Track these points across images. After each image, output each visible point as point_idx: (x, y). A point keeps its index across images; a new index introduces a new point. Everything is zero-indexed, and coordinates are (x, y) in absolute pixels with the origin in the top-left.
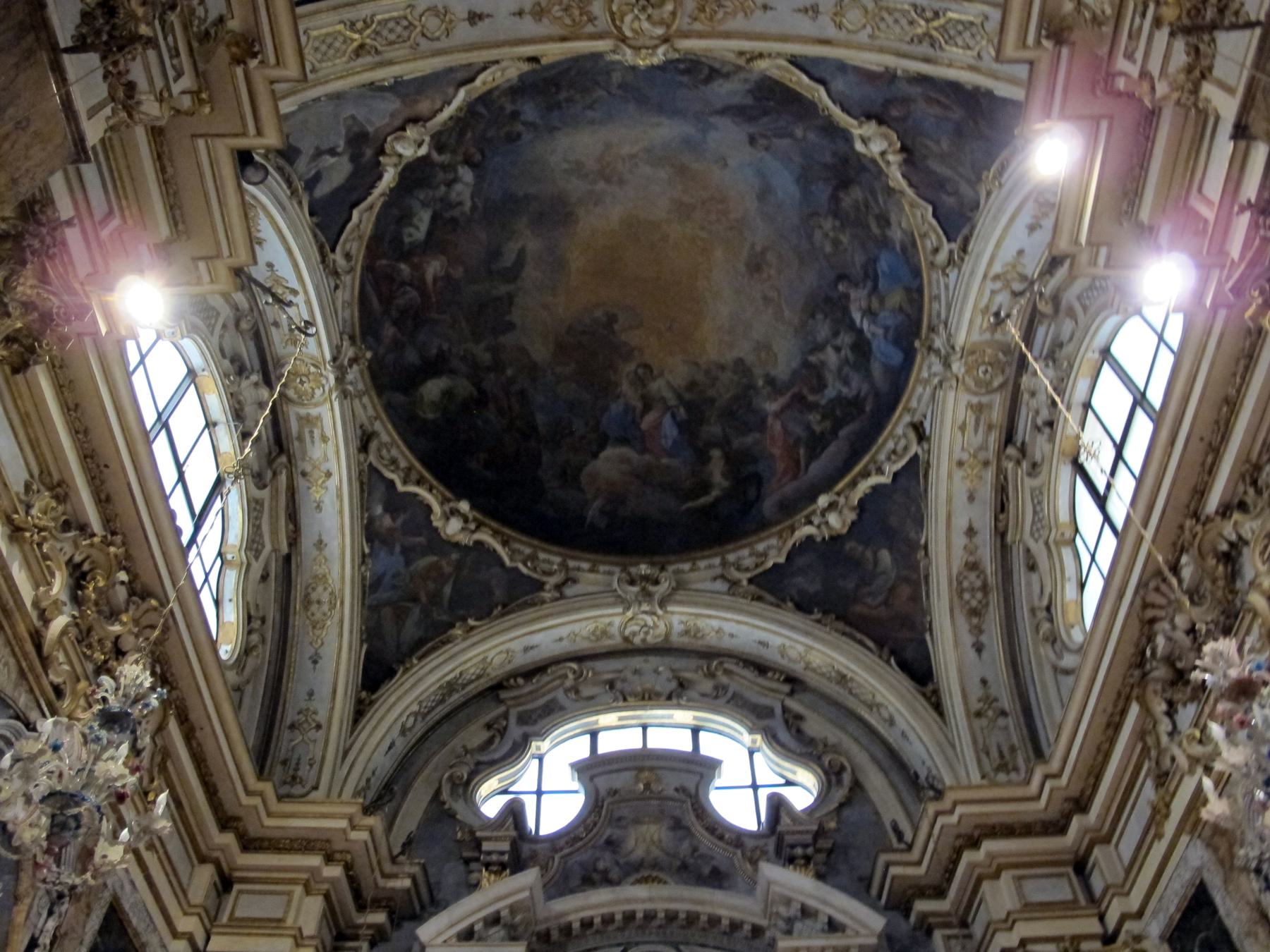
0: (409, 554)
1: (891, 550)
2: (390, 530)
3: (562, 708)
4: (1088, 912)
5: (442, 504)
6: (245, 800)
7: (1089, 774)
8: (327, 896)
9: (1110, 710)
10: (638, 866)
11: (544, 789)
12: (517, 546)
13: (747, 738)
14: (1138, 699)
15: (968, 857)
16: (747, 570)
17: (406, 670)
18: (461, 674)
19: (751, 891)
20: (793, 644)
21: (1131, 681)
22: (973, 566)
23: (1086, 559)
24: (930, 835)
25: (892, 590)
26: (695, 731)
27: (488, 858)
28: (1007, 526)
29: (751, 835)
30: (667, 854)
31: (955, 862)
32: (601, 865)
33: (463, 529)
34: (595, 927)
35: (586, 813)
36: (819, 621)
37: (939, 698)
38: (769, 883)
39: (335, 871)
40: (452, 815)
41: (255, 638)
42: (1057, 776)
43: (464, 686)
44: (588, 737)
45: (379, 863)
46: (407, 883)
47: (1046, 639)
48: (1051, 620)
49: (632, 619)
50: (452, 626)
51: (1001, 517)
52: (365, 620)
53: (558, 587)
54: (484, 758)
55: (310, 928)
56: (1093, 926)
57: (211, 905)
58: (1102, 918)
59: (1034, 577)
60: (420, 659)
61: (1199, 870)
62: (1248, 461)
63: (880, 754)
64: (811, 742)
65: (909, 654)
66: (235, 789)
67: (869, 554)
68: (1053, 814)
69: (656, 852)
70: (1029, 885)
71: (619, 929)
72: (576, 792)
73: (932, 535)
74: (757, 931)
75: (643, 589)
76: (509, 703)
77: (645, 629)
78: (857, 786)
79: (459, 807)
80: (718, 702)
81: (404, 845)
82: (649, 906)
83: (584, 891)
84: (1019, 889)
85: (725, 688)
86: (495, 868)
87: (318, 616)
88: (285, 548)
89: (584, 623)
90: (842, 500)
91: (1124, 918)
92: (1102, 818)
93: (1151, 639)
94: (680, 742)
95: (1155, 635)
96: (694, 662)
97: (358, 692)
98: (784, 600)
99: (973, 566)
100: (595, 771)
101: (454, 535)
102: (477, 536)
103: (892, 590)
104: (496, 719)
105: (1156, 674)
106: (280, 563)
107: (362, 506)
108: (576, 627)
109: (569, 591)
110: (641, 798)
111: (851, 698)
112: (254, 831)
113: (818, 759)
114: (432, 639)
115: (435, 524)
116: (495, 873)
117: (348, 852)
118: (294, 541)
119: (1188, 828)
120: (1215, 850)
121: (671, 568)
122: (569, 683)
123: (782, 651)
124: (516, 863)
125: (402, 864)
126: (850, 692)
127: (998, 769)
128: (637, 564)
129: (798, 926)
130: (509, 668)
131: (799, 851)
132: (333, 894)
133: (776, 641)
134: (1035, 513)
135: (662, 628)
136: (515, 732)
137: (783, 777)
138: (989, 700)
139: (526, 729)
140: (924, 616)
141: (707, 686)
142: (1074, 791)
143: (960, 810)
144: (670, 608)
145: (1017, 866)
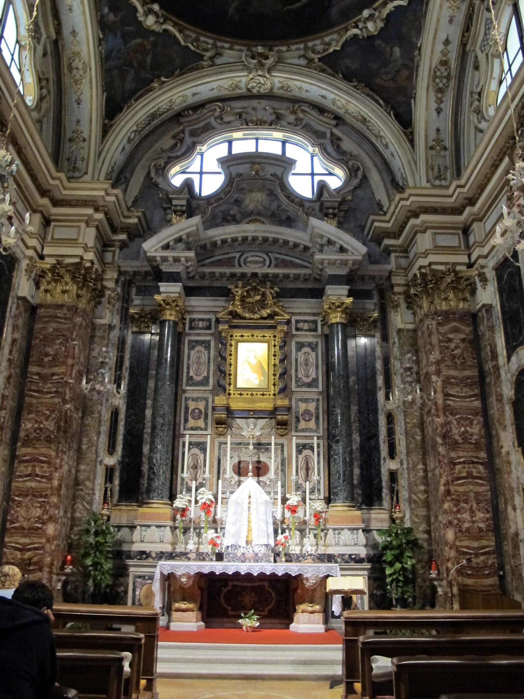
0: (126, 37)
1: (400, 47)
2: (114, 22)
3: (213, 128)
5: (143, 6)
6: (52, 182)
8: (97, 228)
9: (495, 157)
10: (251, 213)
11: (204, 171)
12: (188, 32)
13: (311, 149)
14: (509, 155)
15: (413, 221)
16: (318, 53)
17: (129, 107)
18: (159, 109)
19: (305, 229)
20: (340, 99)
21: (508, 145)
24: (394, 212)
25: (398, 71)
26: (284, 143)
27: (176, 208)
28: (468, 40)
30: (265, 208)
31: (406, 223)
32: (232, 213)
33: (156, 22)
34: (228, 243)
35: (224, 186)
36: (355, 87)
37: (413, 136)
38: (313, 227)
39: (100, 216)
40: (156, 185)
41: (44, 91)
42: (463, 186)
43: (160, 115)
44: (227, 144)
45: (122, 212)
46: (136, 220)
47: (475, 111)
48: (479, 101)
49: (252, 79)
50: (152, 81)
51: (466, 34)
52: (104, 79)
53: (211, 58)
54: (171, 155)
55: (91, 244)
56: (464, 259)
57: (42, 232)
58: (469, 256)
59: (477, 73)
60: (136, 100)
63: (379, 161)
64: (343, 153)
66: (46, 177)
67: (388, 49)
68: (458, 204)
69: (260, 208)
70: (439, 237)
71: (240, 244)
72: (220, 173)
73: (424, 42)
74: (306, 249)
75: (260, 62)
76: (185, 124)
77: (259, 85)
78: (365, 178)
79: (159, 180)
80: (296, 128)
81: (133, 202)
82: (254, 234)
83: (223, 226)
84: (434, 240)
85: (301, 120)
86: (179, 213)
87: (78, 77)
88: (54, 36)
89: (226, 81)
90: (377, 14)
91: (479, 257)
92: (481, 209)
94: (274, 148)
96: (285, 105)
97: (104, 120)
99: (444, 63)
100: (230, 163)
101: (151, 26)
102: (165, 27)
103: (398, 71)
104: (178, 133)
106: (52, 44)
107: (96, 7)
108: (221, 83)
109: (218, 61)
110: (253, 178)
111: (367, 131)
112: (58, 196)
113: (346, 163)
114: (140, 90)
115: (140, 19)
116: (179, 216)
117: (106, 206)
118: (59, 31)
121: (276, 49)
122: (217, 114)
123: (334, 102)
124: (190, 212)
125: (133, 211)
126: (368, 128)
127: (436, 178)
128: (257, 46)
129: (326, 248)
130: (184, 105)
131: (331, 211)
132: (100, 227)
133: (331, 96)
134: (485, 34)
135: (268, 85)
136: (188, 140)
137: (327, 170)
138: (438, 141)
139: (194, 139)
141: (291, 118)
142: (469, 195)
144: (273, 74)
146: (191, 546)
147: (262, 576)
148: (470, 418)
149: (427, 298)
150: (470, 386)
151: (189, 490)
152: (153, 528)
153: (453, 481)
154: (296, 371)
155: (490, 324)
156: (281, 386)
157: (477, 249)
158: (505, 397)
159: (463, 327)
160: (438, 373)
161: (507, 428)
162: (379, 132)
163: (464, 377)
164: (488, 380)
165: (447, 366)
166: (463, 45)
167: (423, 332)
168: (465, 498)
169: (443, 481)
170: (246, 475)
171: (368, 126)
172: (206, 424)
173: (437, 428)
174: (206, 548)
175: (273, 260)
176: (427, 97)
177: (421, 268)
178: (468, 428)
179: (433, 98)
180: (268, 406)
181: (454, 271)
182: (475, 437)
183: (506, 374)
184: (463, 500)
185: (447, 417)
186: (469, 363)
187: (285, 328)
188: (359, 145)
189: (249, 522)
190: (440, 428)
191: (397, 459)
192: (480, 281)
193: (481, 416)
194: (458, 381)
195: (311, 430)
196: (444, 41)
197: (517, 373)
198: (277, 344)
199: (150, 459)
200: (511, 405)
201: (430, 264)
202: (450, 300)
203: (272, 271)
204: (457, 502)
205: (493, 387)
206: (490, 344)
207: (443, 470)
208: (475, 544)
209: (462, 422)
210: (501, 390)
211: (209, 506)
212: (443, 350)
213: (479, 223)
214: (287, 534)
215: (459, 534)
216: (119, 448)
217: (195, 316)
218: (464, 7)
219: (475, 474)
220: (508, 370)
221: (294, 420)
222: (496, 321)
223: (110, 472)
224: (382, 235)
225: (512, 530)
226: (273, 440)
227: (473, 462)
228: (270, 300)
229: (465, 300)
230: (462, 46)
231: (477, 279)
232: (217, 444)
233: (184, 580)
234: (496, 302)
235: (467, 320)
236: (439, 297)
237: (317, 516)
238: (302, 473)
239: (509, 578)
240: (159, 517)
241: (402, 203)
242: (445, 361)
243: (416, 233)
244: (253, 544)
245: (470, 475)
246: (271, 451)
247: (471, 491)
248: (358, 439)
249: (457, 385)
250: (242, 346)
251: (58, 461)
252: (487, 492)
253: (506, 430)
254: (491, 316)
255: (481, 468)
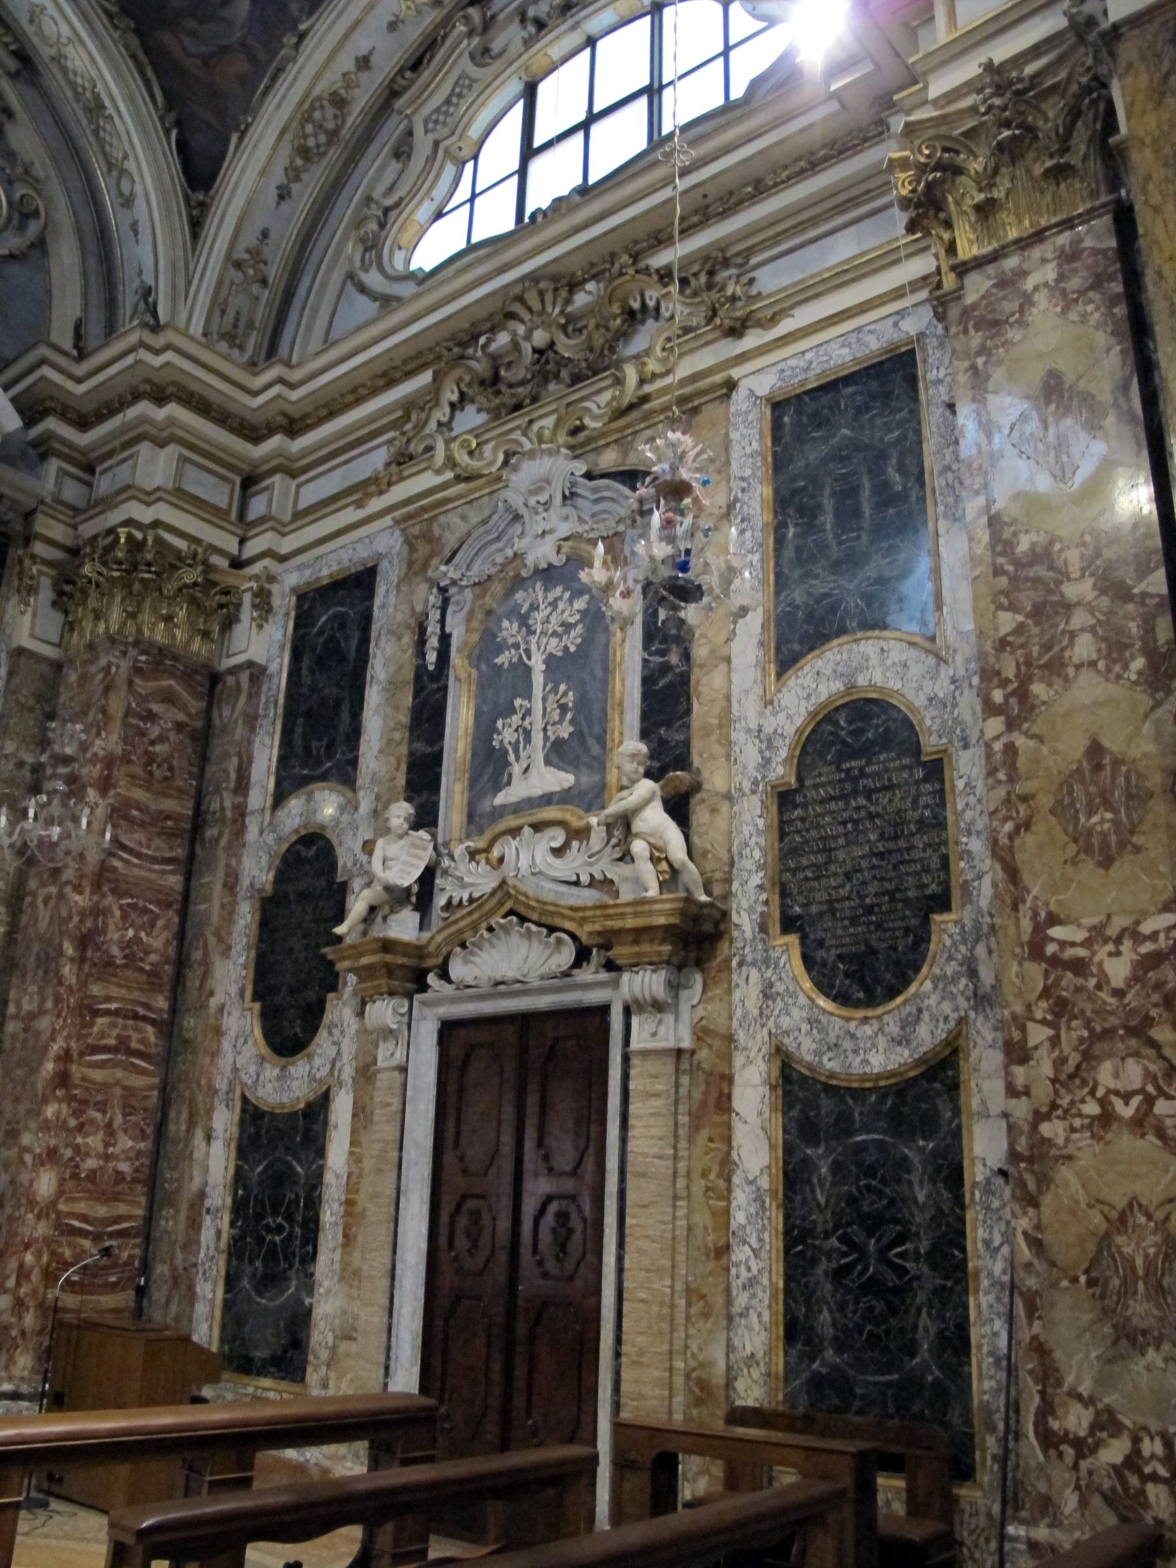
4: (233, 529)
7: (326, 405)
9: (397, 362)
14: (435, 374)
15: (143, 408)
20: (58, 17)
22: (339, 102)
23: (463, 192)
25: (225, 50)
28: (406, 89)
42: (292, 386)
47: (363, 240)
48: (382, 226)
51: (408, 74)
58: (242, 541)
59: (394, 166)
61: (381, 556)
62: (722, 250)
65: (198, 141)
70: (191, 472)
73: (320, 28)
78: (40, 245)
84: (179, 473)
91: (268, 553)
93: (494, 330)
95: (504, 328)
99: (339, 102)
105: (473, 364)
111: (92, 139)
119: (397, 514)
120: (412, 549)
126: (96, 133)
134: (448, 102)
140: (246, 112)
142: (295, 412)
143: (169, 356)
145: (192, 447)
148: (151, 911)
149: (123, 600)
150: (170, 835)
153: (81, 1054)
155: (250, 711)
157: (269, 534)
158: (246, 882)
159: (185, 695)
160: (105, 785)
161: (233, 952)
162: (126, 157)
163: (161, 812)
164: (210, 832)
165: (132, 776)
166: (392, 93)
167: (84, 678)
168: (100, 1098)
169: (56, 1048)
171: (98, 127)
173: (70, 917)
176: (274, 149)
177: (129, 522)
178: (143, 934)
179: (282, 160)
181: (205, 563)
182: (153, 957)
183: (261, 832)
184: (96, 1104)
185: (104, 896)
186: (179, 783)
188: (54, 159)
190: (76, 919)
192: (254, 606)
193: (176, 911)
194: (147, 819)
196: (360, 55)
197: (294, 838)
200: (257, 904)
201: (156, 524)
202: (176, 626)
204: (80, 1106)
205: (221, 855)
206: (240, 755)
207: (61, 1021)
208: (101, 1211)
209: (133, 916)
210: (239, 862)
212: (132, 734)
213: (288, 479)
215: (70, 1184)
218: (432, 16)
219: (134, 1045)
220: (270, 823)
222: (266, 708)
224: (48, 404)
225: (195, 1185)
227: (136, 1017)
229: (206, 634)
230: (387, 92)
231: (247, 598)
234: (279, 667)
235: (200, 684)
236: (155, 610)
239: (158, 1294)
241: (143, 354)
242: (129, 761)
243: (138, 439)
245: (122, 1046)
247: (118, 1082)
249: (143, 825)
252: (152, 1089)
253: (228, 957)
254: (258, 694)
255: (150, 1031)
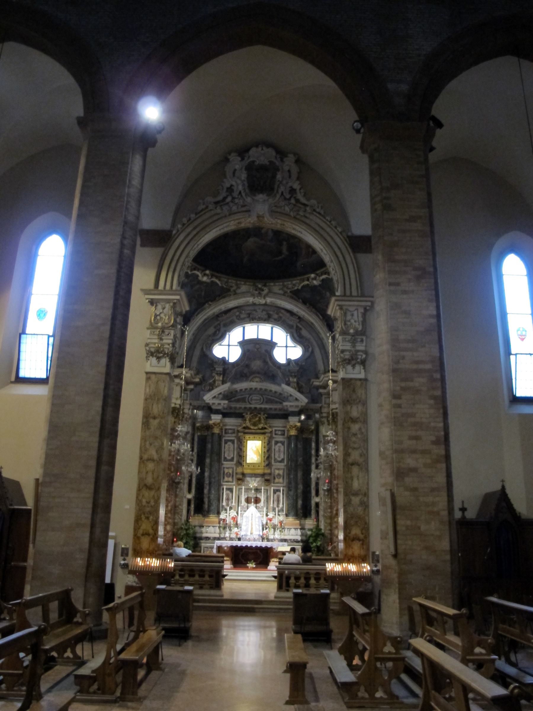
16: (289, 289)
17: (193, 319)
29: (283, 365)
32: (245, 372)
79: (208, 353)
85: (281, 317)
98: (299, 299)
109: (239, 291)
131: (293, 374)
136: (222, 329)
141: (276, 316)
146: (227, 535)
147: (256, 547)
151: (226, 510)
152: (211, 527)
154: (274, 455)
156: (267, 463)
170: (251, 503)
172: (233, 480)
174: (233, 536)
175: (265, 399)
180: (260, 471)
187: (269, 435)
189: (252, 525)
191: (319, 497)
195: (280, 483)
198: (266, 442)
199: (209, 497)
203: (263, 406)
211: (235, 518)
214: (268, 530)
216: (193, 490)
217: (227, 427)
221: (272, 478)
223: (189, 502)
226: (263, 488)
228: (263, 421)
232: (238, 489)
233: (226, 548)
237: (281, 523)
238: (276, 503)
240: (213, 522)
244: (253, 534)
246: (262, 493)
248: (302, 487)
250: (249, 442)
251: (170, 499)
